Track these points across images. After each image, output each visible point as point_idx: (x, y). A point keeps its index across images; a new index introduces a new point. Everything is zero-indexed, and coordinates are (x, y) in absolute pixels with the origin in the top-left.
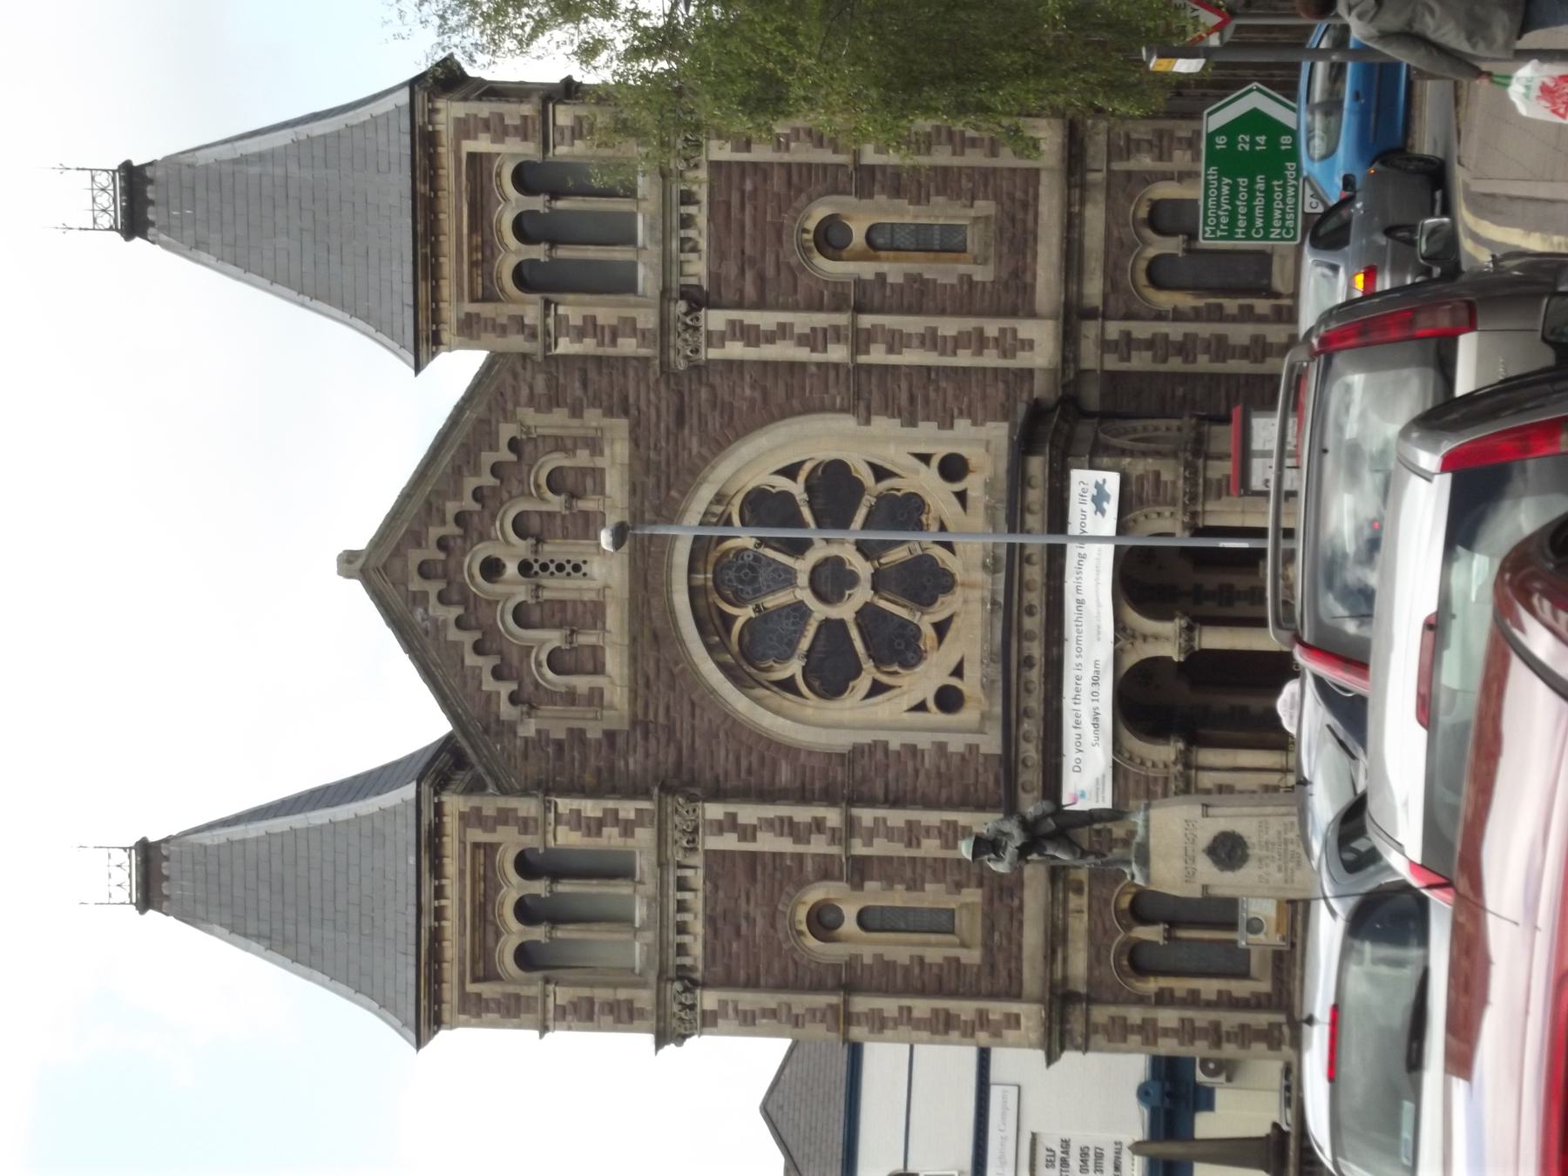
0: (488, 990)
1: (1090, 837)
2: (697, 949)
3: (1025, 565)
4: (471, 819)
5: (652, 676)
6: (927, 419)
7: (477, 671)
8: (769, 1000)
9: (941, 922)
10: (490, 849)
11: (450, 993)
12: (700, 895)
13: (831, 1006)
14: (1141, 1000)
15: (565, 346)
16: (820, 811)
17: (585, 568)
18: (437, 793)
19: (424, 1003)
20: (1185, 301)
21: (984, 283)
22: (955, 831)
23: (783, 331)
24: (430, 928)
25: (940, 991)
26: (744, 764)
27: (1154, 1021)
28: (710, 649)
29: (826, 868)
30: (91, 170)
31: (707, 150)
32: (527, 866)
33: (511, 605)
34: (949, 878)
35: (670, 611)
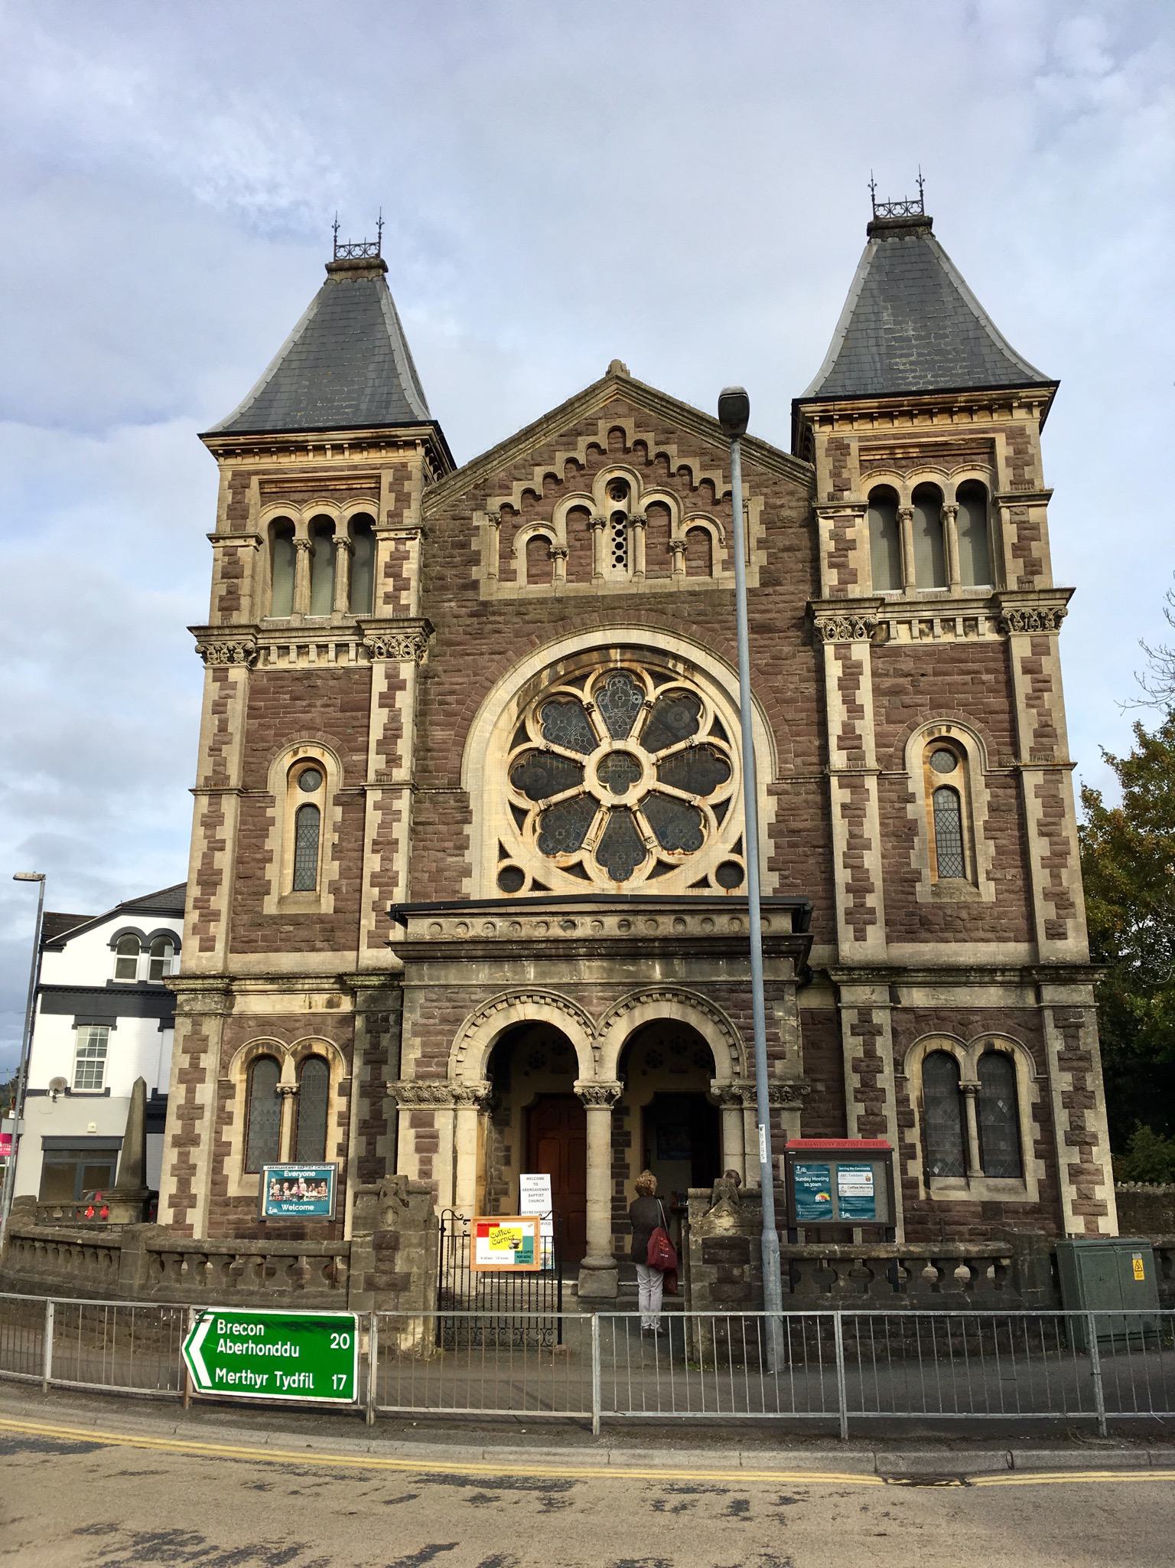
0: (253, 493)
1: (381, 1011)
2: (283, 664)
3: (673, 917)
4: (401, 472)
5: (527, 617)
6: (777, 847)
7: (530, 477)
8: (236, 724)
9: (304, 881)
10: (376, 493)
11: (250, 463)
12: (332, 665)
13: (228, 778)
14: (225, 1067)
15: (825, 526)
16: (407, 761)
17: (620, 566)
18: (424, 442)
19: (242, 439)
20: (914, 1089)
21: (914, 894)
22: (387, 885)
23: (854, 710)
24: (307, 441)
25: (240, 877)
26: (450, 698)
27: (202, 1081)
28: (552, 665)
29: (354, 772)
30: (922, 200)
31: (1019, 636)
32: (362, 525)
33: (587, 503)
34: (344, 882)
35: (587, 629)
